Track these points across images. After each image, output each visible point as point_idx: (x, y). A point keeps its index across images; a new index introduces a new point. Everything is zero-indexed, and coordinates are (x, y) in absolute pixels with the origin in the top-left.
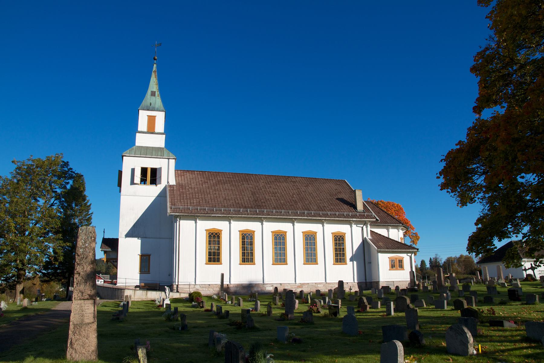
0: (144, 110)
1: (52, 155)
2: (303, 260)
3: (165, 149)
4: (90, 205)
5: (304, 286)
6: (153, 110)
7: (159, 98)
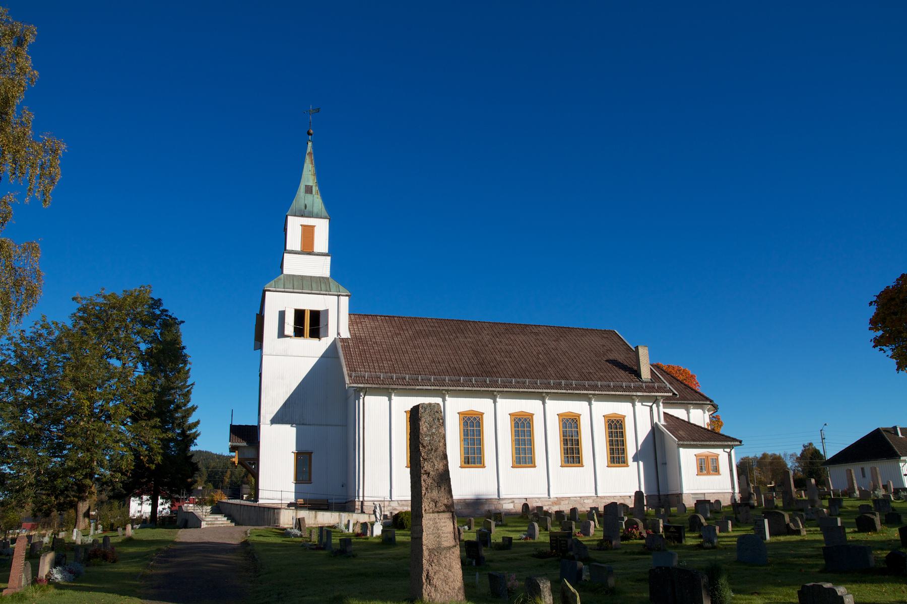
1: (134, 286)
2: (552, 458)
3: (331, 280)
5: (562, 503)
6: (311, 215)
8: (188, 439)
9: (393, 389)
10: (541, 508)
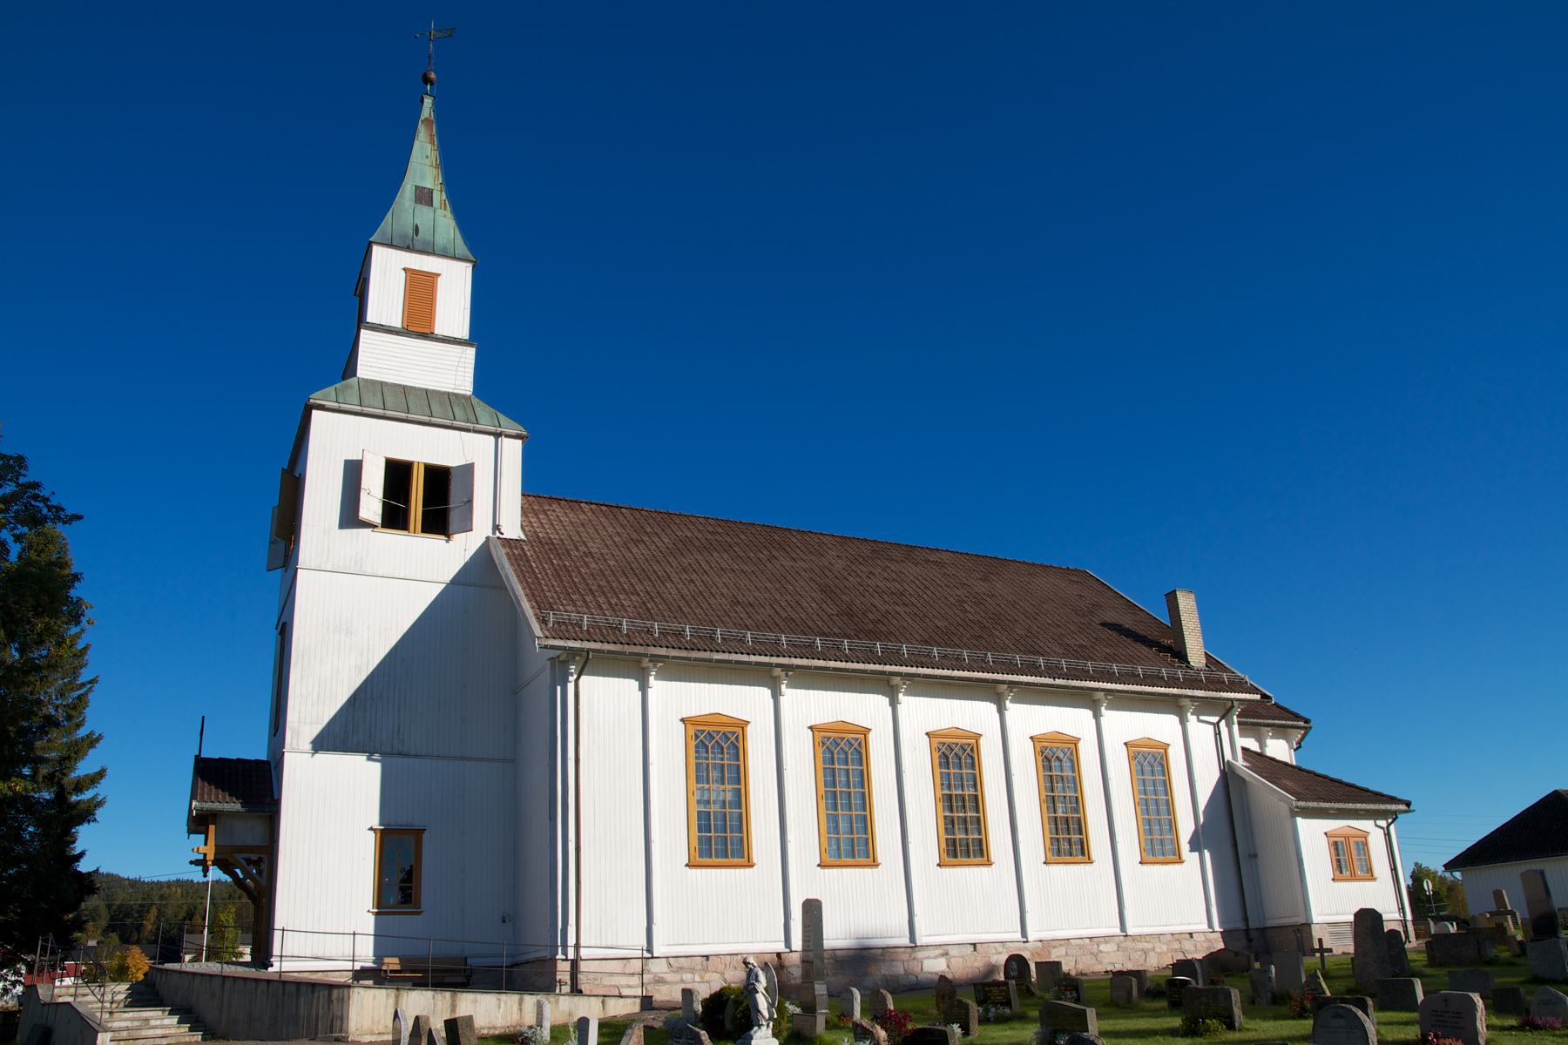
0: (391, 246)
3: (475, 401)
4: (85, 649)
6: (429, 250)
7: (448, 213)
8: (69, 814)
9: (655, 659)
10: (1058, 964)
